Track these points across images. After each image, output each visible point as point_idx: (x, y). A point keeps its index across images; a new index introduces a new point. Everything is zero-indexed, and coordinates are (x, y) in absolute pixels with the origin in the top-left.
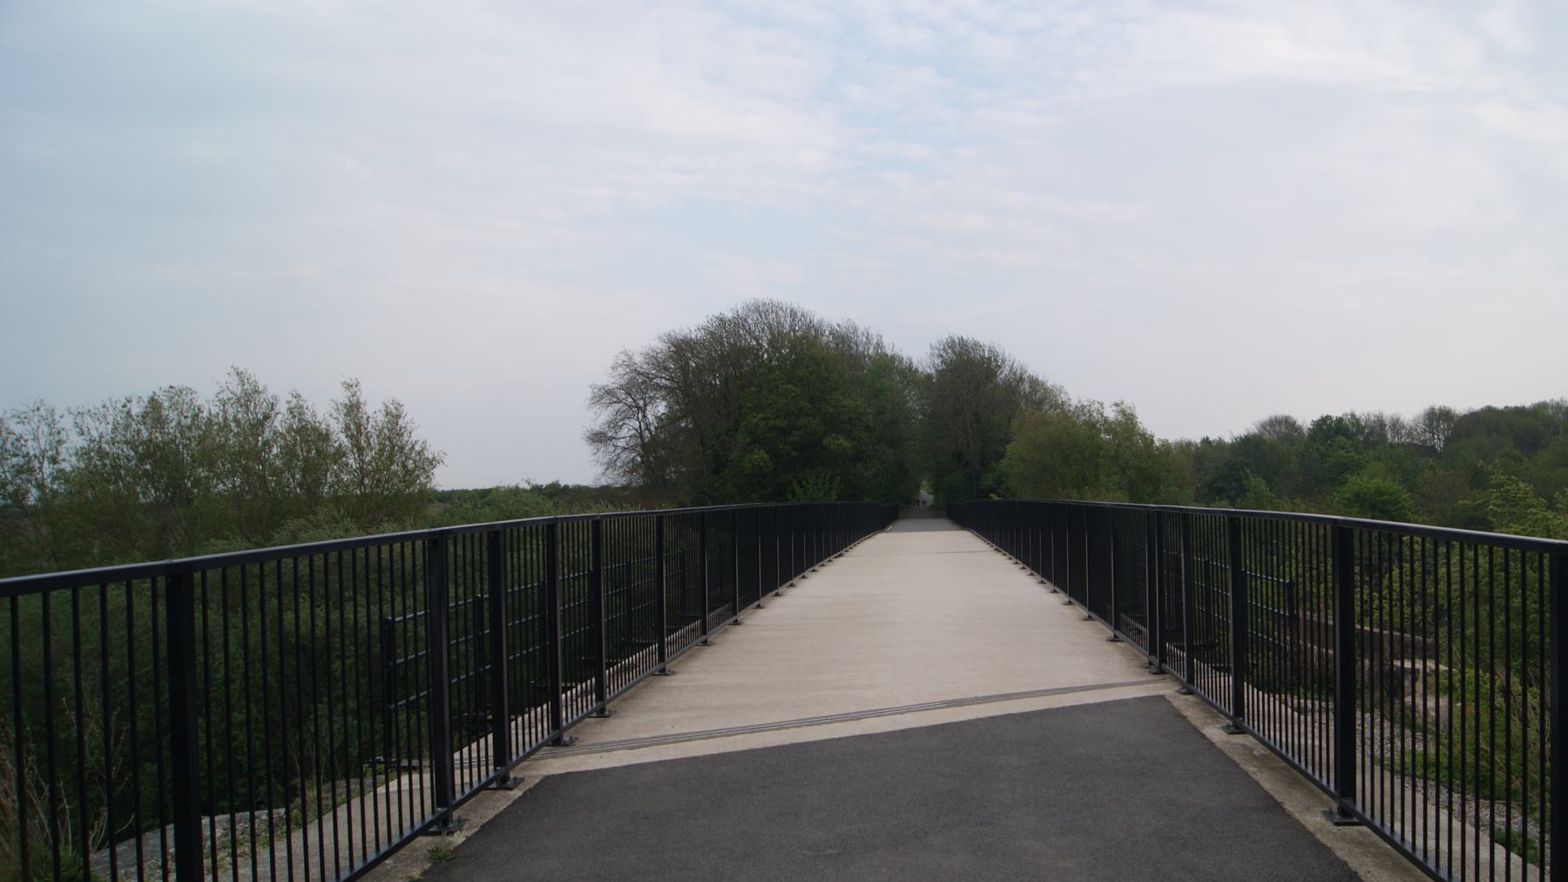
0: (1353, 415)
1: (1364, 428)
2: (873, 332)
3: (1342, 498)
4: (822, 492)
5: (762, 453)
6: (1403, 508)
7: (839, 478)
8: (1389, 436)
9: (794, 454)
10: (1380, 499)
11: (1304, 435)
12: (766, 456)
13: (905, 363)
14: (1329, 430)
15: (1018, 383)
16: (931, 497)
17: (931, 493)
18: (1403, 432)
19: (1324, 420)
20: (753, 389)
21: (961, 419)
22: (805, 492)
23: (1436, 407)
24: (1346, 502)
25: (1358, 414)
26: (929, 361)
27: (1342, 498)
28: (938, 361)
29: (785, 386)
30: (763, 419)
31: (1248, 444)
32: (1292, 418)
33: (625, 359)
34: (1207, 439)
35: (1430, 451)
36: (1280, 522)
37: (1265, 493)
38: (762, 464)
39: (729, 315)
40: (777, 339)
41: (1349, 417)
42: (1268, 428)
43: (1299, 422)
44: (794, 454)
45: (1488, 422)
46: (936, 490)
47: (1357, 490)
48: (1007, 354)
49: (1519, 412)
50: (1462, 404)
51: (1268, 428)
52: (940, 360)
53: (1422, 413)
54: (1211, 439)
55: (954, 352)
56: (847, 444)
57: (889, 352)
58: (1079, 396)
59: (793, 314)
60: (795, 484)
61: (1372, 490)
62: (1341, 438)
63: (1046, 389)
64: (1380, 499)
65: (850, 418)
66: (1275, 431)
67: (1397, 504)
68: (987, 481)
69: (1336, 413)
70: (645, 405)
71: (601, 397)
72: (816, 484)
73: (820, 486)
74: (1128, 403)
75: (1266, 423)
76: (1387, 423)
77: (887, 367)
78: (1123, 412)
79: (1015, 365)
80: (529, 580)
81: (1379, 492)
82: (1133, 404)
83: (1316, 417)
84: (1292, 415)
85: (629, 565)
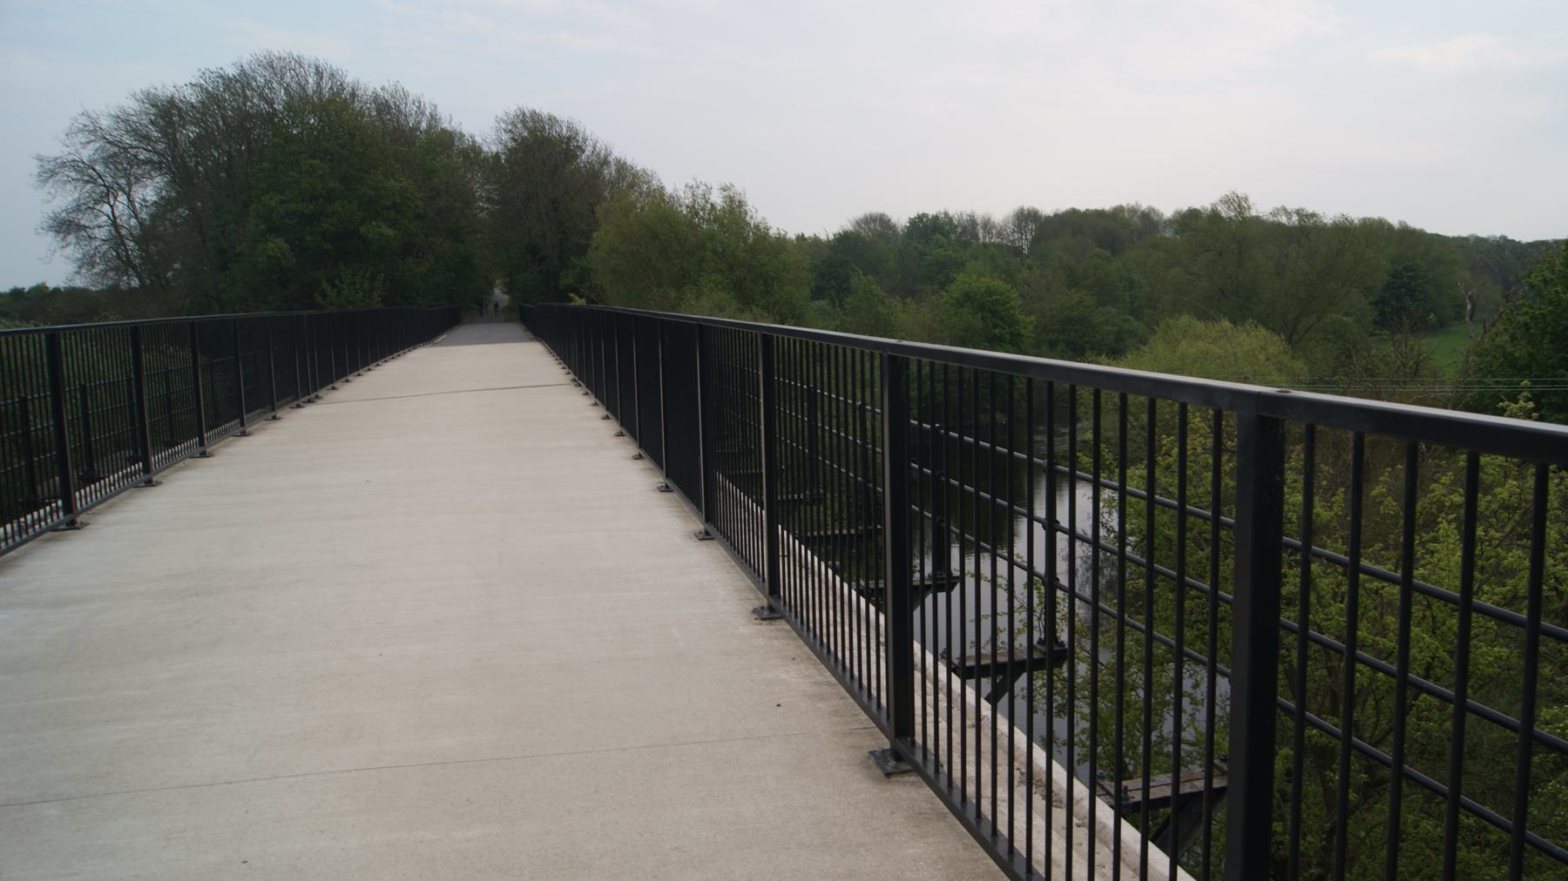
0: (946, 214)
1: (956, 227)
2: (426, 100)
3: (952, 298)
4: (361, 293)
5: (281, 242)
6: (1013, 308)
7: (383, 275)
8: (981, 236)
9: (327, 246)
10: (990, 299)
11: (898, 233)
12: (286, 246)
13: (467, 143)
14: (929, 229)
15: (602, 166)
16: (507, 297)
17: (507, 293)
18: (994, 232)
19: (921, 217)
20: (266, 165)
21: (534, 206)
22: (338, 293)
23: (1025, 208)
24: (955, 302)
25: (951, 213)
26: (494, 137)
27: (952, 298)
28: (505, 137)
29: (310, 161)
30: (282, 202)
31: (845, 240)
32: (887, 216)
33: (87, 123)
34: (803, 235)
35: (1017, 251)
36: (120, 329)
37: (876, 292)
38: (279, 255)
39: (231, 71)
40: (300, 103)
41: (943, 216)
42: (863, 225)
43: (894, 220)
44: (327, 246)
45: (1074, 224)
46: (509, 289)
47: (967, 289)
48: (588, 133)
49: (1100, 214)
50: (1049, 205)
51: (863, 225)
52: (510, 135)
53: (1011, 214)
54: (806, 236)
55: (525, 127)
56: (390, 232)
57: (446, 125)
58: (674, 184)
59: (319, 73)
60: (325, 284)
61: (983, 290)
62: (938, 236)
63: (635, 176)
64: (990, 299)
65: (394, 203)
66: (869, 228)
67: (1005, 304)
68: (567, 279)
69: (931, 211)
70: (129, 185)
71: (53, 173)
72: (353, 283)
73: (358, 286)
74: (738, 188)
75: (860, 220)
76: (979, 222)
77: (443, 142)
78: (731, 199)
79: (598, 145)
80: (92, 379)
81: (989, 292)
82: (744, 190)
83: (913, 215)
84: (886, 213)
85: (24, 401)
